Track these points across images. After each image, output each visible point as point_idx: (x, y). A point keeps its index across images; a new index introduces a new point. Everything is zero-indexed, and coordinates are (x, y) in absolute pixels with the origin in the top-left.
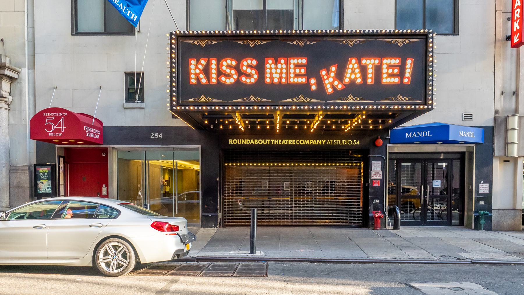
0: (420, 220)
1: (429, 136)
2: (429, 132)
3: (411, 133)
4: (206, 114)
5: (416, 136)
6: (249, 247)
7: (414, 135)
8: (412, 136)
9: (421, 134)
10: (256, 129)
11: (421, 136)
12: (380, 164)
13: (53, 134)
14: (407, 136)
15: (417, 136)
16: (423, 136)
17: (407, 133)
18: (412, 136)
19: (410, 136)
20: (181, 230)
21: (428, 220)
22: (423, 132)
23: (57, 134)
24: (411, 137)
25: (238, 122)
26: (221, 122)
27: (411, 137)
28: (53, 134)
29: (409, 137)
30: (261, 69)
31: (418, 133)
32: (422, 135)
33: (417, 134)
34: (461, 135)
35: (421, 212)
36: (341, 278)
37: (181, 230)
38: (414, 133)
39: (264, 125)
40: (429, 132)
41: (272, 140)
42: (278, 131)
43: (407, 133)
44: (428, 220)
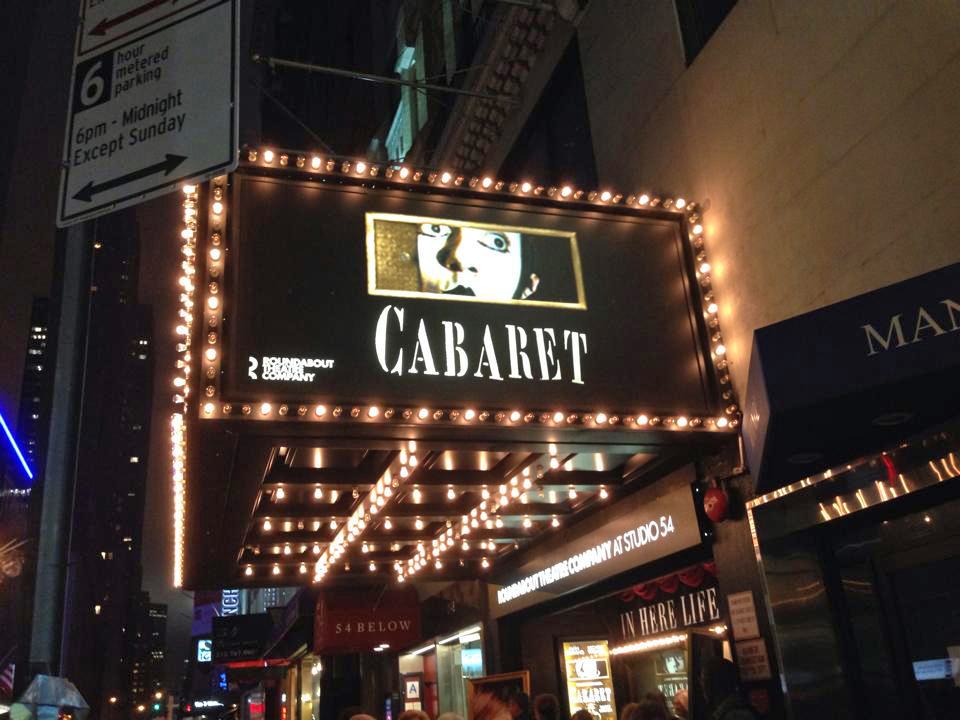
0: (844, 581)
3: (895, 320)
5: (940, 331)
6: (543, 445)
7: (923, 322)
12: (751, 604)
13: (377, 627)
14: (875, 341)
18: (908, 336)
23: (392, 626)
24: (902, 342)
27: (902, 342)
28: (377, 627)
29: (886, 345)
35: (827, 591)
38: (923, 313)
42: (28, 491)
43: (869, 328)
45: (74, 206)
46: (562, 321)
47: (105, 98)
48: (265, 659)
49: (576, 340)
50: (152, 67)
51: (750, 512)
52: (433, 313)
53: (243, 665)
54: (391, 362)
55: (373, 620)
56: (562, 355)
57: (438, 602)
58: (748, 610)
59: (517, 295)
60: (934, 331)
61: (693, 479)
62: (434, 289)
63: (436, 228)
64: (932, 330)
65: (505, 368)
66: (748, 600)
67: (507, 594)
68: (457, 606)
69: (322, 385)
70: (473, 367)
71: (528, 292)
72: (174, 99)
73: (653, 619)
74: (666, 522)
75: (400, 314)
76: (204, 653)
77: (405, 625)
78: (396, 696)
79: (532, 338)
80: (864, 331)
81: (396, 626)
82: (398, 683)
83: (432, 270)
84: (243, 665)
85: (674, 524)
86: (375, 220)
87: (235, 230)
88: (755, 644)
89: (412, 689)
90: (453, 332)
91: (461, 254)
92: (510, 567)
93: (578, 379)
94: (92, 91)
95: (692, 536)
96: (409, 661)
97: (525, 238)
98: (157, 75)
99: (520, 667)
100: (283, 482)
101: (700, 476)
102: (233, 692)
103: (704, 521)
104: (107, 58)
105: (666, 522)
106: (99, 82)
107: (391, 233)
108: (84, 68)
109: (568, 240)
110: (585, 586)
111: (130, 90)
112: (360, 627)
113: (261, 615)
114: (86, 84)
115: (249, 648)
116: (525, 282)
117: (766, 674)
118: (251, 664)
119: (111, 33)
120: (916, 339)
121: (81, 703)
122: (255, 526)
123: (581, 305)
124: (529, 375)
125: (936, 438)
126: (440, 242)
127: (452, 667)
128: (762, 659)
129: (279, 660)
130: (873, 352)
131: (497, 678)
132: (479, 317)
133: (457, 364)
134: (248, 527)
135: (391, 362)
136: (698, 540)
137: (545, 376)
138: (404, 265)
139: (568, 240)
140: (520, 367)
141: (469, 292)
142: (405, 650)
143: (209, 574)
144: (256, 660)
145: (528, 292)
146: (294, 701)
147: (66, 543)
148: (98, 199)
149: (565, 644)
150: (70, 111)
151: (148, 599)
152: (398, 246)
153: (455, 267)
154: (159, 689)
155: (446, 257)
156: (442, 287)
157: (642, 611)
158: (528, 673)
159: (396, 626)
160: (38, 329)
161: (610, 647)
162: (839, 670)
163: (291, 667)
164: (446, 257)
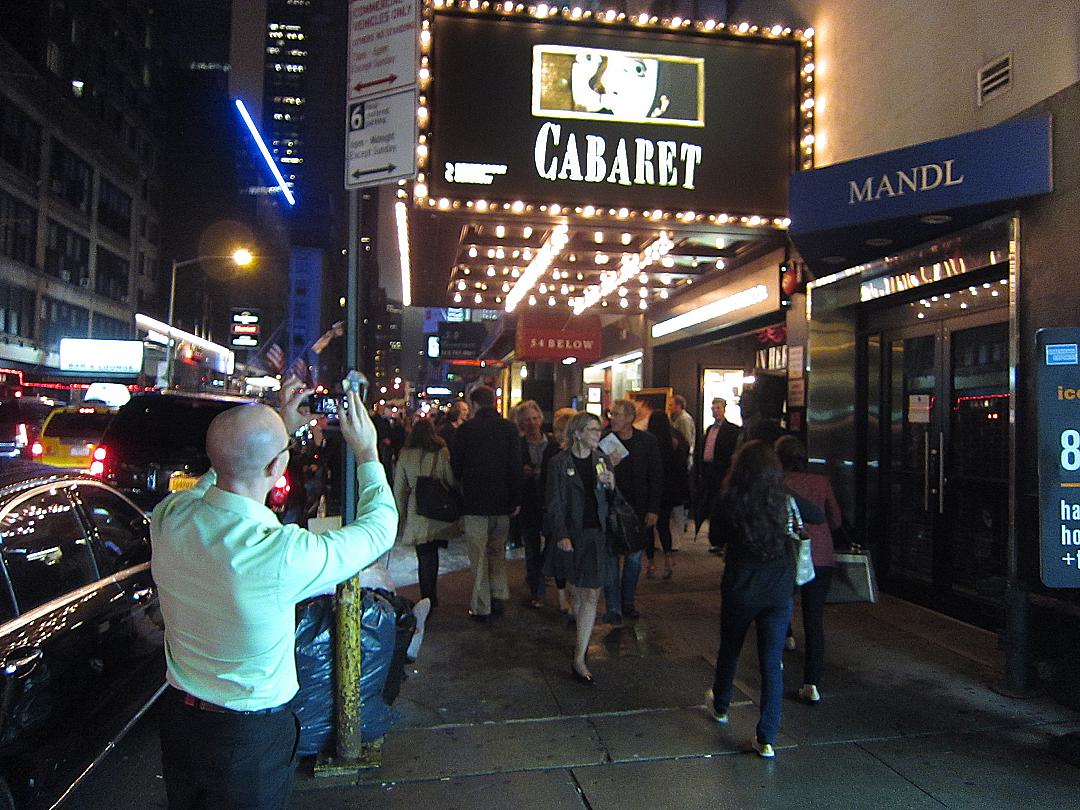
1: (949, 182)
2: (949, 164)
5: (892, 194)
7: (885, 186)
8: (873, 195)
9: (912, 180)
11: (914, 187)
16: (924, 187)
17: (853, 184)
19: (866, 196)
22: (924, 169)
24: (869, 198)
25: (808, 75)
27: (869, 198)
29: (860, 198)
31: (901, 174)
32: (919, 185)
36: (1034, 386)
38: (885, 179)
40: (949, 164)
42: (193, 67)
43: (853, 184)
45: (353, 180)
46: (681, 136)
47: (362, 127)
48: (482, 360)
49: (692, 153)
50: (382, 116)
51: (809, 292)
52: (580, 129)
53: (464, 362)
54: (547, 169)
55: (561, 338)
56: (679, 163)
57: (614, 330)
59: (649, 116)
61: (782, 260)
62: (583, 109)
63: (589, 58)
64: (887, 192)
65: (632, 175)
67: (660, 330)
68: (628, 334)
69: (497, 191)
70: (608, 174)
71: (658, 112)
72: (390, 137)
73: (778, 357)
75: (556, 130)
76: (434, 349)
77: (588, 345)
78: (580, 399)
79: (656, 149)
80: (849, 185)
81: (580, 344)
82: (583, 389)
83: (583, 94)
84: (464, 362)
86: (543, 53)
87: (437, 52)
88: (798, 382)
89: (594, 395)
90: (596, 145)
91: (604, 81)
92: (660, 311)
93: (689, 184)
94: (357, 122)
95: (774, 304)
96: (592, 374)
97: (661, 64)
98: (384, 121)
99: (667, 386)
101: (787, 258)
102: (458, 383)
103: (783, 296)
104: (362, 105)
106: (359, 117)
107: (554, 62)
108: (353, 107)
109: (696, 66)
110: (729, 324)
111: (370, 70)
112: (551, 344)
113: (478, 324)
114: (354, 118)
115: (468, 349)
116: (657, 104)
117: (801, 403)
118: (471, 363)
119: (364, 91)
121: (787, 289)
122: (463, 254)
123: (700, 123)
124: (651, 181)
125: (37, 449)
126: (592, 71)
127: (624, 381)
128: (800, 393)
129: (494, 361)
130: (852, 202)
131: (650, 391)
132: (616, 133)
133: (596, 172)
134: (459, 253)
135: (547, 169)
136: (777, 307)
137: (663, 181)
138: (562, 90)
139: (696, 66)
140: (644, 175)
141: (610, 112)
142: (589, 364)
143: (430, 291)
144: (474, 359)
145: (658, 112)
146: (506, 396)
148: (363, 178)
149: (707, 371)
151: (385, 296)
152: (558, 74)
153: (601, 91)
154: (398, 375)
155: (594, 83)
156: (589, 109)
157: (772, 350)
158: (671, 390)
159: (580, 344)
160: (274, 27)
161: (744, 375)
162: (852, 408)
163: (504, 367)
164: (594, 83)
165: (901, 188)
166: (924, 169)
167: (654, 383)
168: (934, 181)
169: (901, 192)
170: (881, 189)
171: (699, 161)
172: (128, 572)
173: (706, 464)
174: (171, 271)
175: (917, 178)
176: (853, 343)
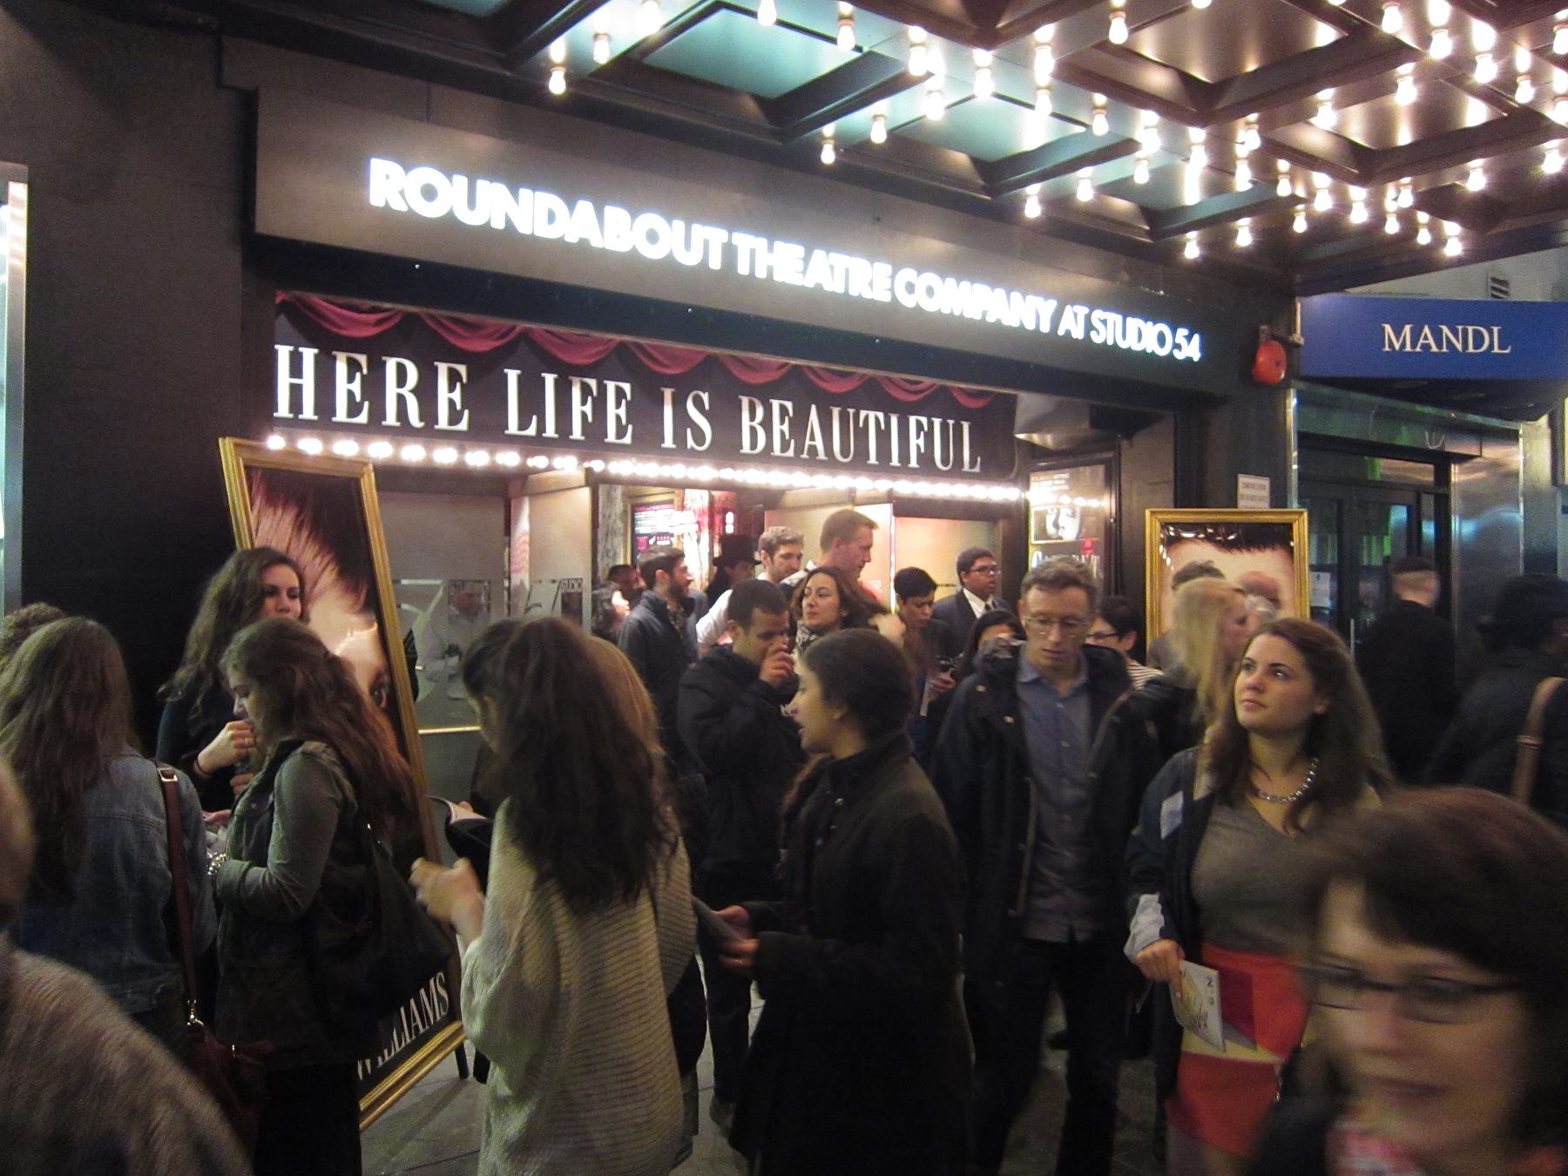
2: (1496, 329)
3: (1407, 328)
4: (1119, 436)
5: (1434, 349)
7: (1426, 338)
10: (235, 887)
11: (1459, 347)
15: (1439, 345)
16: (1471, 349)
17: (1388, 328)
18: (1414, 345)
19: (1403, 345)
20: (871, 284)
21: (1427, 436)
24: (1408, 348)
26: (980, 692)
29: (1397, 346)
30: (1056, 319)
31: (1445, 329)
33: (1437, 336)
34: (1397, 346)
37: (871, 284)
38: (1426, 330)
39: (1016, 469)
40: (1496, 329)
41: (291, 416)
43: (1388, 328)
44: (1427, 436)
58: (1261, 499)
60: (1430, 347)
66: (1263, 487)
74: (1189, 338)
80: (1384, 329)
85: (1203, 348)
100: (100, 620)
105: (1189, 338)
120: (1418, 349)
130: (1387, 349)
147: (1110, 588)
150: (868, 630)
165: (1445, 346)
166: (1470, 329)
167: (1303, 433)
168: (1481, 345)
169: (1445, 350)
170: (1421, 341)
171: (922, 450)
172: (811, 116)
173: (923, 454)
174: (855, 450)
175: (1463, 338)
176: (1403, 428)
